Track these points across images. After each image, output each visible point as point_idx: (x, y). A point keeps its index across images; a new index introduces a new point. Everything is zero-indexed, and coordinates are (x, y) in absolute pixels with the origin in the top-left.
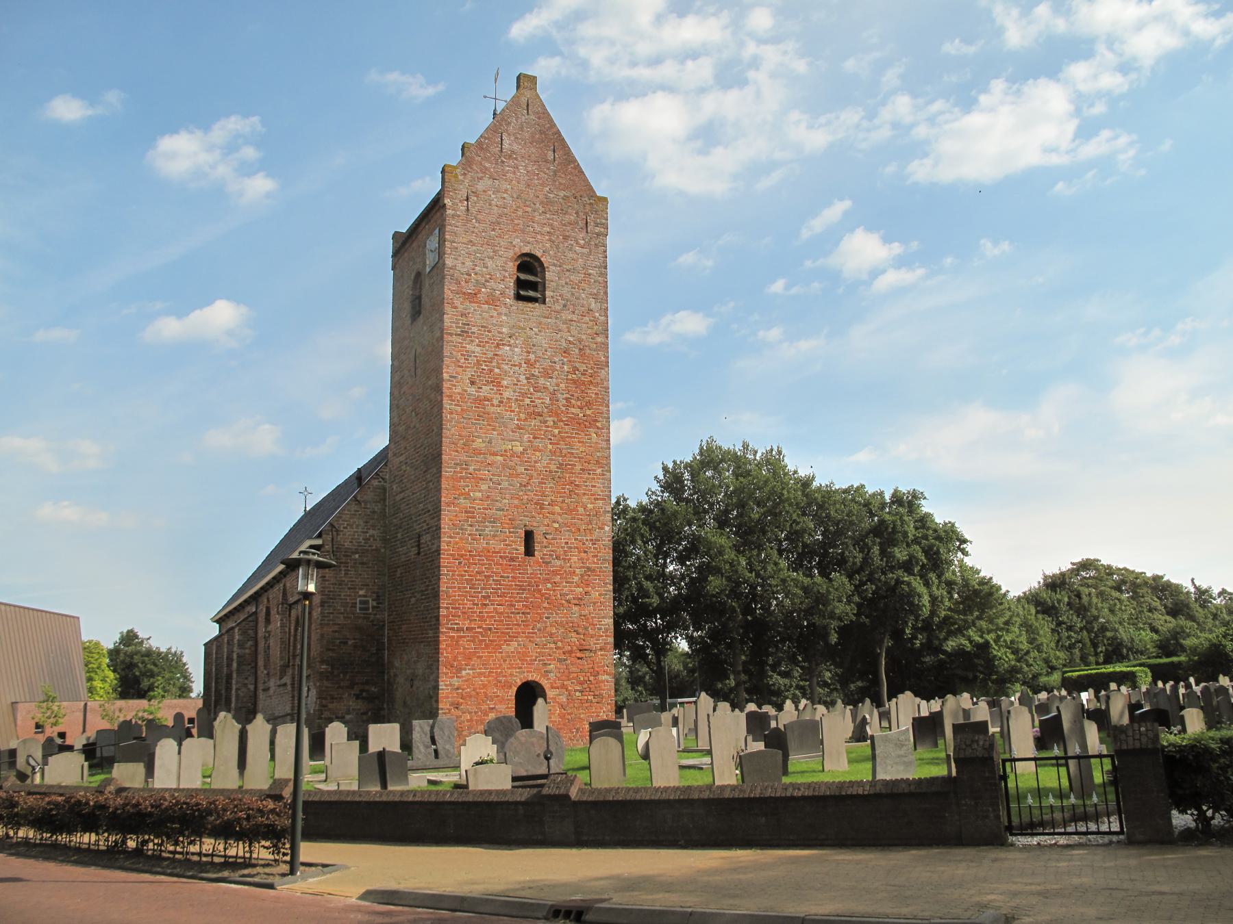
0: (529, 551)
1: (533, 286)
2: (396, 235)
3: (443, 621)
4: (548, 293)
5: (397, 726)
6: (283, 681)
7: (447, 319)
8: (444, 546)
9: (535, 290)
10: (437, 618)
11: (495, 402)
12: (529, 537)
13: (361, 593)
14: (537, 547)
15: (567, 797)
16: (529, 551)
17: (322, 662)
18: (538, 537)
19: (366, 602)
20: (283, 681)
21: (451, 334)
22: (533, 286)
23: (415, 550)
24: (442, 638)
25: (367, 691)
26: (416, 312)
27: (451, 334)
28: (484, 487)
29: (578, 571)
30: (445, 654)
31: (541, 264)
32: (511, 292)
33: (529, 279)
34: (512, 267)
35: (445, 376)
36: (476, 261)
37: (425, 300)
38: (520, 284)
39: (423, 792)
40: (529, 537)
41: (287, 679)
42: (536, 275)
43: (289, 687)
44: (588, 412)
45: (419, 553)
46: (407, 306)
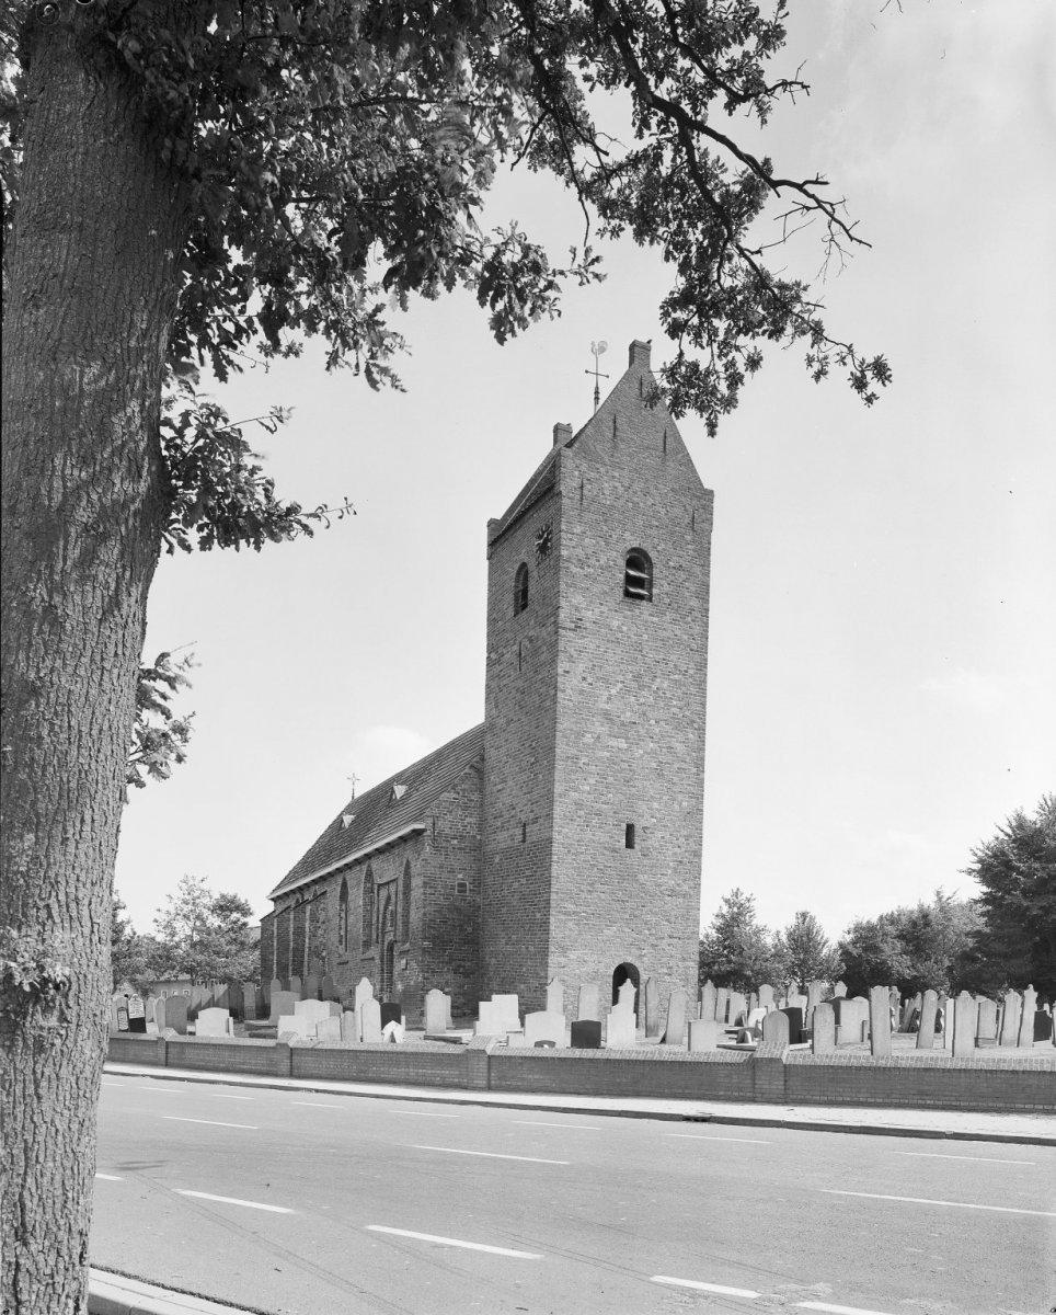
0: (630, 844)
1: (639, 582)
2: (492, 523)
3: (553, 904)
4: (655, 591)
5: (515, 997)
6: (369, 954)
7: (562, 615)
8: (555, 836)
9: (642, 587)
10: (548, 901)
11: (604, 698)
12: (630, 829)
13: (460, 876)
14: (637, 840)
15: (780, 1060)
16: (630, 844)
17: (425, 939)
18: (638, 831)
19: (464, 885)
20: (369, 954)
21: (564, 628)
22: (639, 582)
23: (520, 838)
24: (552, 920)
25: (464, 967)
26: (522, 600)
27: (564, 628)
28: (592, 781)
29: (671, 864)
30: (555, 931)
31: (651, 564)
32: (620, 592)
33: (637, 577)
34: (622, 563)
35: (560, 671)
36: (588, 555)
37: (532, 591)
38: (630, 580)
39: (715, 1055)
40: (630, 829)
41: (374, 952)
42: (642, 572)
43: (378, 961)
44: (687, 713)
45: (524, 841)
46: (509, 598)
